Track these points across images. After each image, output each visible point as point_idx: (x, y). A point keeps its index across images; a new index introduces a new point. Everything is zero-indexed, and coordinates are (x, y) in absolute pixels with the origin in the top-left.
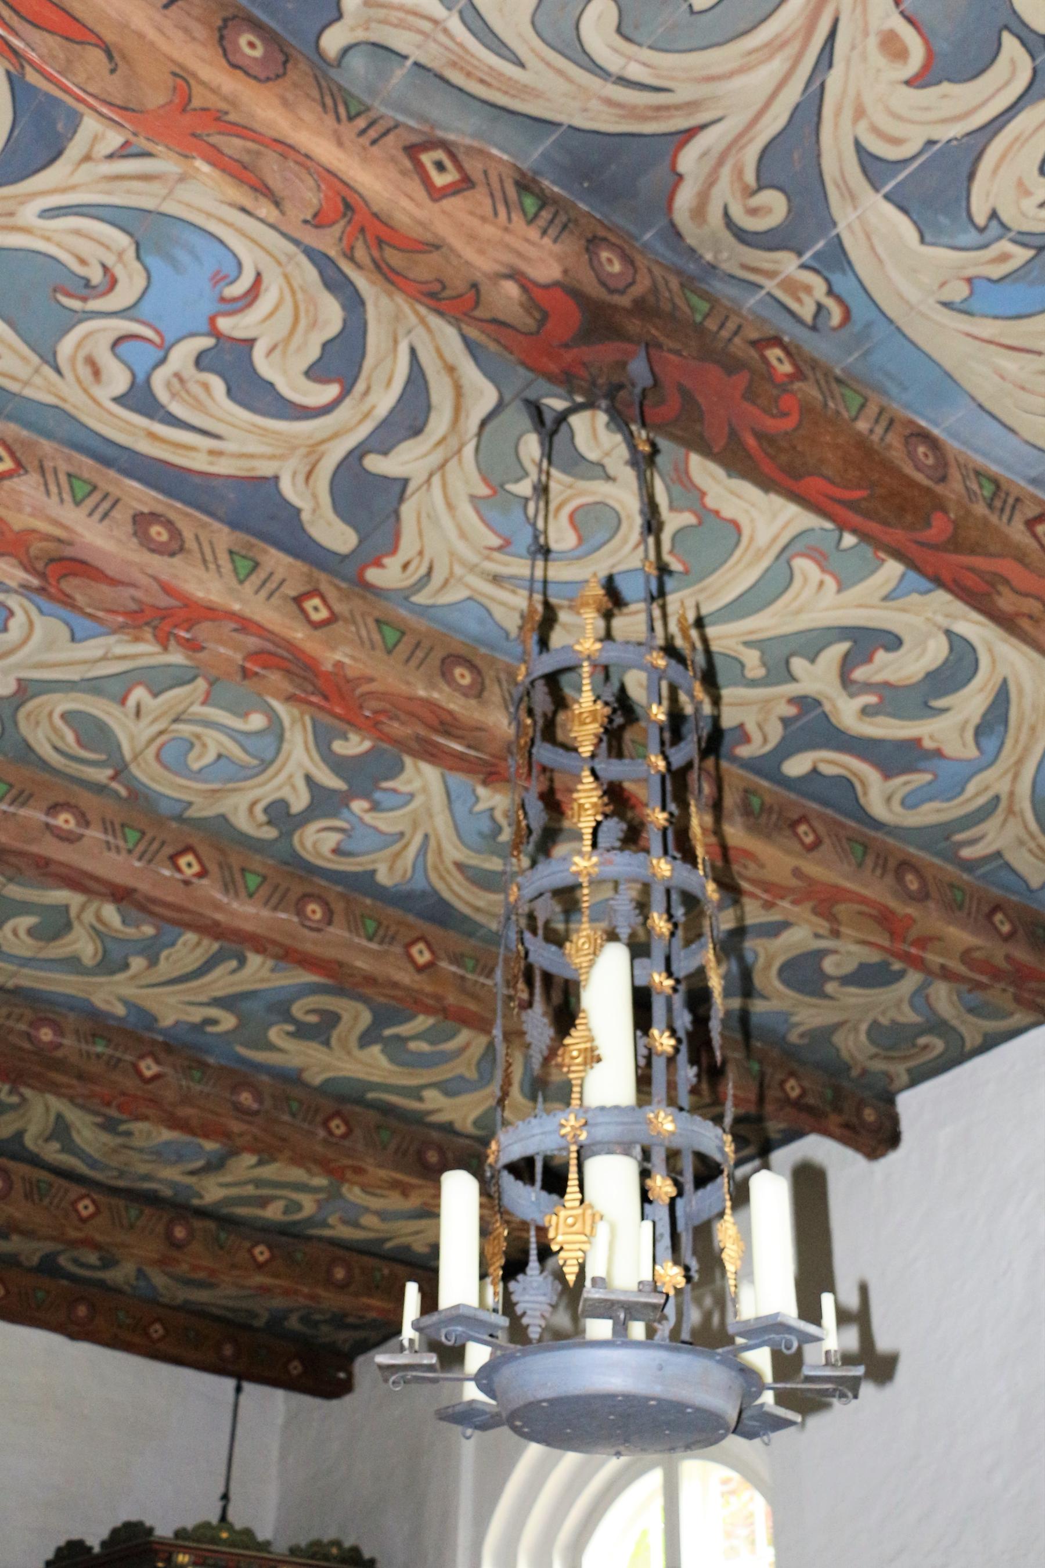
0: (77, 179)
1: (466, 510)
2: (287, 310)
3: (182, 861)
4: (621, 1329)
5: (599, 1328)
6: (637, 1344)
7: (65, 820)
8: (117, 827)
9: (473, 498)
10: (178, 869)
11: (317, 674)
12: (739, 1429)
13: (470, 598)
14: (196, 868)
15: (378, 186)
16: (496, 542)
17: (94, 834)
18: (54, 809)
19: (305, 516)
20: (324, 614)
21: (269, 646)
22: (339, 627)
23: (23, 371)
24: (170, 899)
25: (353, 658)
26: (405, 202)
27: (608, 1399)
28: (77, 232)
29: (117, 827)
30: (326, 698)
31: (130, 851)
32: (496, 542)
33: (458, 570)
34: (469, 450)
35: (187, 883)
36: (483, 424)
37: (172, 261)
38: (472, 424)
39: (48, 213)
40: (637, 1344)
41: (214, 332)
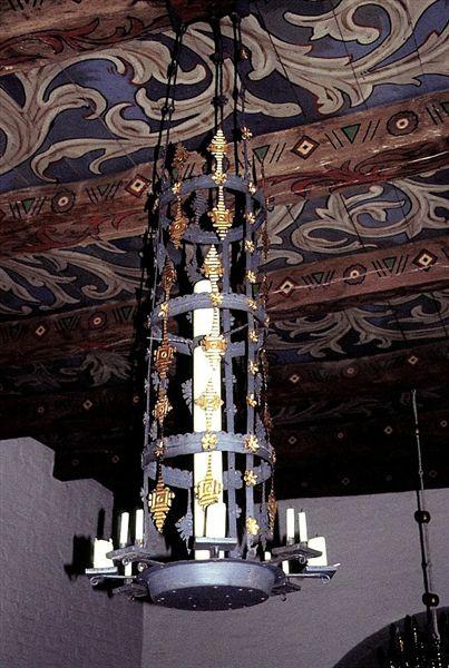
0: (34, 82)
1: (311, 60)
2: (144, 59)
3: (421, 261)
4: (214, 555)
5: (201, 555)
6: (221, 560)
7: (354, 274)
8: (381, 262)
9: (308, 54)
10: (421, 265)
11: (320, 176)
12: (275, 592)
13: (374, 86)
14: (430, 259)
15: (53, 21)
16: (347, 60)
17: (371, 272)
18: (346, 273)
19: (265, 113)
20: (311, 146)
21: (293, 180)
22: (321, 148)
23: (118, 148)
24: (424, 281)
25: (331, 160)
26: (67, 16)
27: (209, 589)
28: (59, 97)
29: (381, 262)
30: (344, 181)
31: (391, 271)
32: (347, 60)
33: (353, 81)
34: (275, 41)
35: (426, 270)
36: (263, 26)
37: (91, 79)
38: (260, 31)
39: (46, 98)
40: (221, 560)
41: (139, 87)
